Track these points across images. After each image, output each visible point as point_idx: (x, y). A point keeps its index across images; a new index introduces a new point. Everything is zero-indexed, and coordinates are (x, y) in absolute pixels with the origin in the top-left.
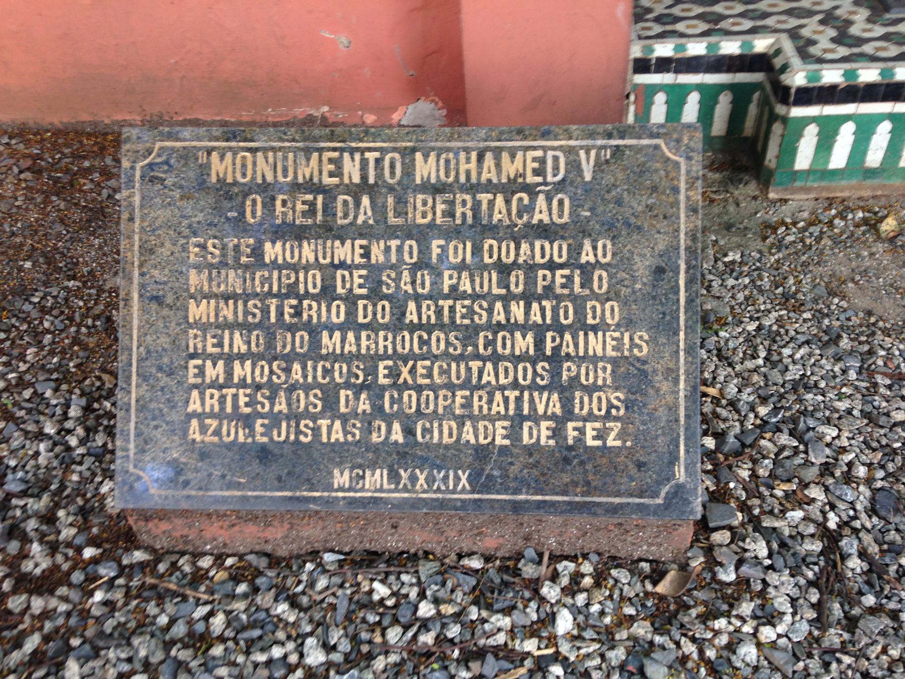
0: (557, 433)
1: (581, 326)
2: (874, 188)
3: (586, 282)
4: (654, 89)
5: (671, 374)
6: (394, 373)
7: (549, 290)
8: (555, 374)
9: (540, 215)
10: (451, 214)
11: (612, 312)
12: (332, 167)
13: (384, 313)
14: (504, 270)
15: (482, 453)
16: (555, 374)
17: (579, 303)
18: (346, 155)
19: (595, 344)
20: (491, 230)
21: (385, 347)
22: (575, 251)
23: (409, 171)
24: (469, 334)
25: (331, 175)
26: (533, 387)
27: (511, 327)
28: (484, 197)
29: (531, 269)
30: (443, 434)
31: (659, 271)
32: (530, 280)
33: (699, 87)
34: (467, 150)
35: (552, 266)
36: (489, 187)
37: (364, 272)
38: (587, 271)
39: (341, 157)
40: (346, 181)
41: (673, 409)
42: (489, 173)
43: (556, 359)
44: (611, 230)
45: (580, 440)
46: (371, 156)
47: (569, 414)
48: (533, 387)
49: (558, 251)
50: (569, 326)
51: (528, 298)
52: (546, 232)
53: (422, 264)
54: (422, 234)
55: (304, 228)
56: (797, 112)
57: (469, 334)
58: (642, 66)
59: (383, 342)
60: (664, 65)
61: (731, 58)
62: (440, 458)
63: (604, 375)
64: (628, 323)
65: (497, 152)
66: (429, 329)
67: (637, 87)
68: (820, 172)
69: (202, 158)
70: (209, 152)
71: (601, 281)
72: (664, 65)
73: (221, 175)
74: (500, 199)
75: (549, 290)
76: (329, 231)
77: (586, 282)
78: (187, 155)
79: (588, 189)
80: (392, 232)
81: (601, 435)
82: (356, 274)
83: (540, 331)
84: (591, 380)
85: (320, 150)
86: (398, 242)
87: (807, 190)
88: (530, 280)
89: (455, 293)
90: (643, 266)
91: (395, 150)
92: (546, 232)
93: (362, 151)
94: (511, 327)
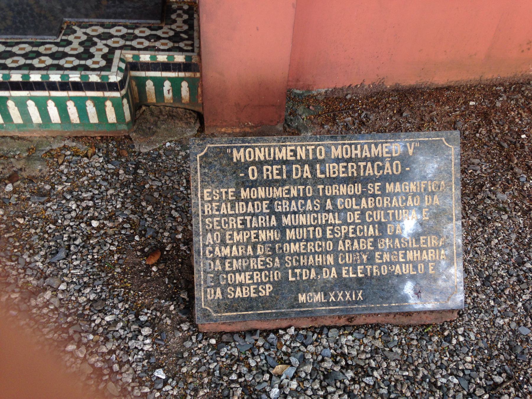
10: (346, 172)
12: (344, 169)
18: (299, 148)
21: (262, 224)
25: (343, 172)
28: (362, 164)
34: (356, 145)
36: (365, 159)
37: (359, 212)
39: (296, 148)
40: (350, 175)
46: (310, 148)
50: (310, 197)
55: (277, 181)
65: (369, 145)
69: (229, 151)
70: (232, 148)
73: (238, 159)
74: (369, 164)
76: (289, 181)
78: (223, 150)
82: (356, 213)
84: (297, 223)
85: (286, 146)
86: (322, 186)
91: (322, 145)
93: (306, 146)
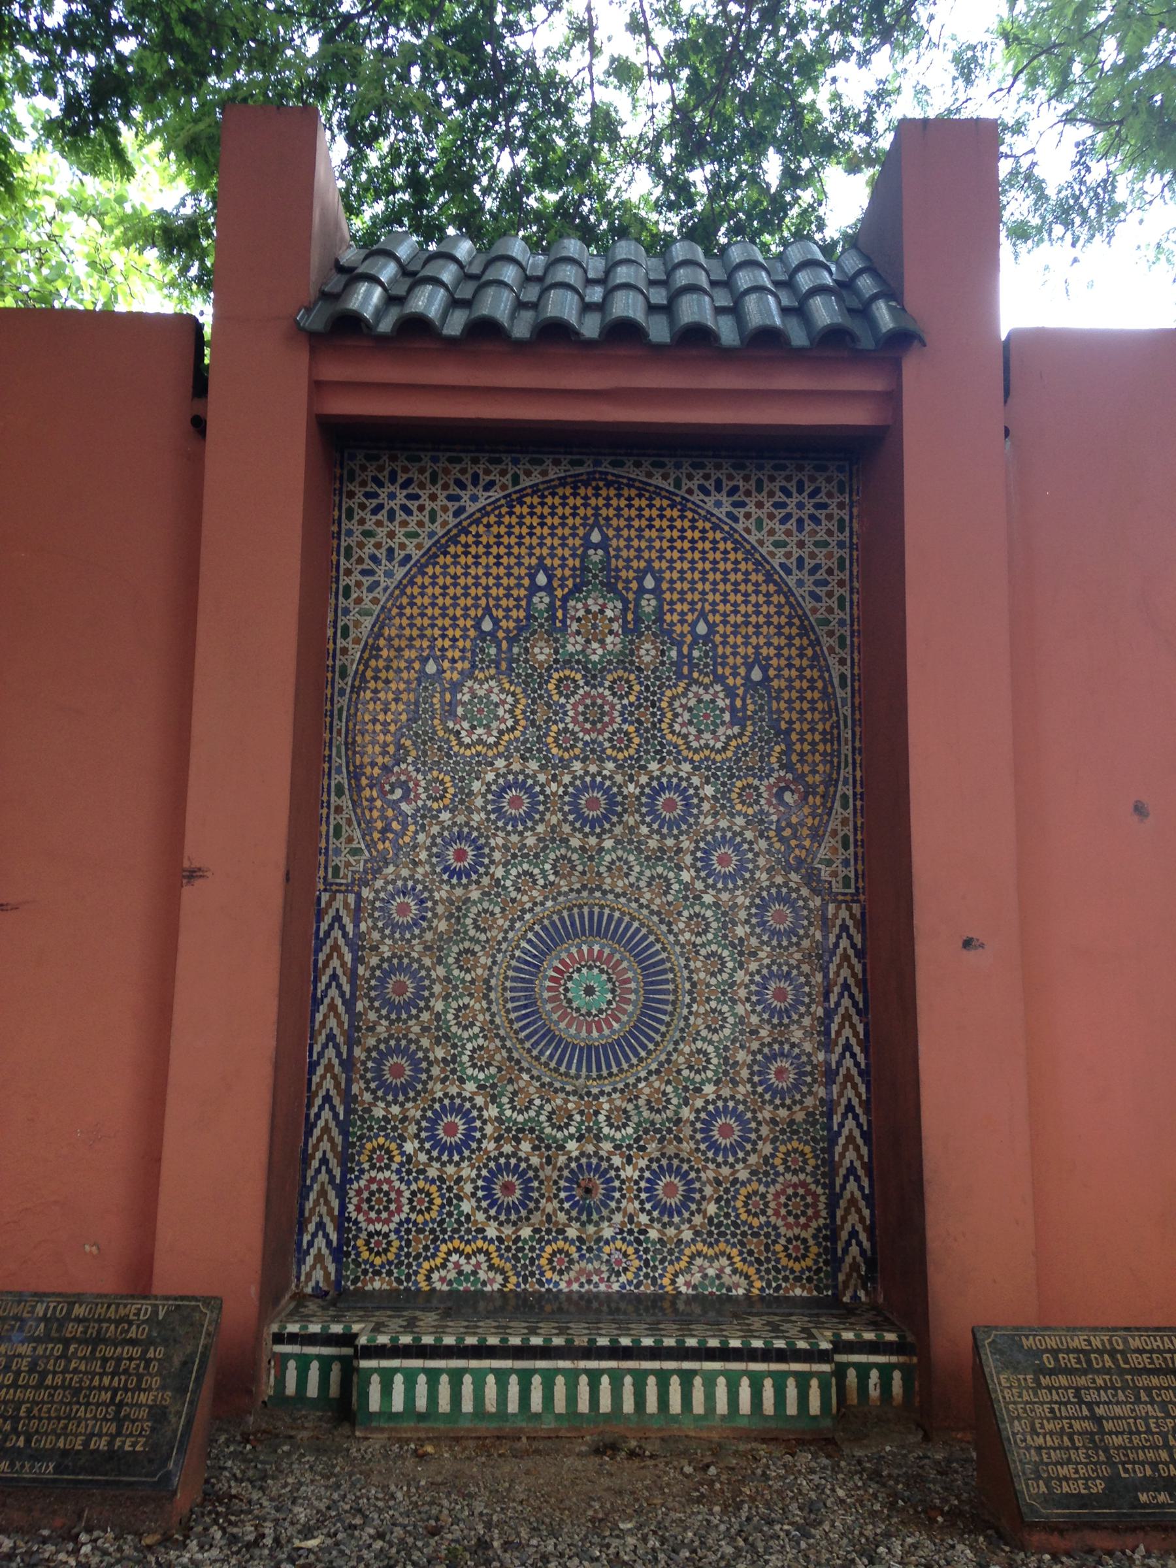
0: (110, 1443)
1: (139, 1388)
2: (427, 1430)
3: (147, 1367)
4: (286, 1357)
5: (179, 1414)
6: (29, 1411)
7: (126, 1371)
8: (118, 1412)
9: (132, 1334)
11: (156, 1382)
13: (34, 1379)
14: (105, 1360)
15: (65, 1453)
16: (118, 1412)
17: (140, 1378)
19: (143, 1398)
20: (105, 1341)
22: (145, 1352)
23: (69, 1312)
24: (77, 1392)
26: (105, 1419)
27: (101, 1388)
29: (119, 1360)
30: (46, 1443)
31: (184, 1363)
32: (118, 1365)
33: (319, 1357)
35: (131, 1359)
36: (110, 1320)
38: (148, 1362)
41: (175, 1431)
42: (111, 1313)
43: (121, 1405)
44: (165, 1342)
45: (121, 1447)
47: (119, 1433)
48: (105, 1419)
49: (136, 1352)
51: (113, 1374)
52: (133, 1342)
53: (64, 1355)
54: (67, 1342)
56: (364, 1364)
57: (77, 1392)
58: (279, 1338)
59: (30, 1394)
60: (293, 1339)
61: (336, 1335)
62: (38, 1456)
63: (144, 1413)
64: (163, 1388)
66: (56, 1388)
67: (275, 1354)
68: (387, 1414)
71: (154, 1367)
72: (293, 1339)
75: (126, 1371)
77: (147, 1367)
79: (159, 1323)
80: (51, 1340)
81: (134, 1445)
83: (115, 1391)
87: (382, 1430)
88: (118, 1365)
89: (76, 1371)
90: (176, 1362)
92: (133, 1342)
94: (101, 1388)
